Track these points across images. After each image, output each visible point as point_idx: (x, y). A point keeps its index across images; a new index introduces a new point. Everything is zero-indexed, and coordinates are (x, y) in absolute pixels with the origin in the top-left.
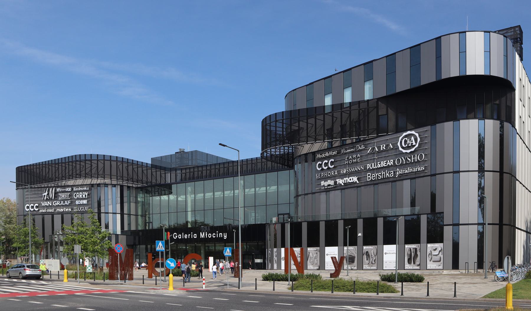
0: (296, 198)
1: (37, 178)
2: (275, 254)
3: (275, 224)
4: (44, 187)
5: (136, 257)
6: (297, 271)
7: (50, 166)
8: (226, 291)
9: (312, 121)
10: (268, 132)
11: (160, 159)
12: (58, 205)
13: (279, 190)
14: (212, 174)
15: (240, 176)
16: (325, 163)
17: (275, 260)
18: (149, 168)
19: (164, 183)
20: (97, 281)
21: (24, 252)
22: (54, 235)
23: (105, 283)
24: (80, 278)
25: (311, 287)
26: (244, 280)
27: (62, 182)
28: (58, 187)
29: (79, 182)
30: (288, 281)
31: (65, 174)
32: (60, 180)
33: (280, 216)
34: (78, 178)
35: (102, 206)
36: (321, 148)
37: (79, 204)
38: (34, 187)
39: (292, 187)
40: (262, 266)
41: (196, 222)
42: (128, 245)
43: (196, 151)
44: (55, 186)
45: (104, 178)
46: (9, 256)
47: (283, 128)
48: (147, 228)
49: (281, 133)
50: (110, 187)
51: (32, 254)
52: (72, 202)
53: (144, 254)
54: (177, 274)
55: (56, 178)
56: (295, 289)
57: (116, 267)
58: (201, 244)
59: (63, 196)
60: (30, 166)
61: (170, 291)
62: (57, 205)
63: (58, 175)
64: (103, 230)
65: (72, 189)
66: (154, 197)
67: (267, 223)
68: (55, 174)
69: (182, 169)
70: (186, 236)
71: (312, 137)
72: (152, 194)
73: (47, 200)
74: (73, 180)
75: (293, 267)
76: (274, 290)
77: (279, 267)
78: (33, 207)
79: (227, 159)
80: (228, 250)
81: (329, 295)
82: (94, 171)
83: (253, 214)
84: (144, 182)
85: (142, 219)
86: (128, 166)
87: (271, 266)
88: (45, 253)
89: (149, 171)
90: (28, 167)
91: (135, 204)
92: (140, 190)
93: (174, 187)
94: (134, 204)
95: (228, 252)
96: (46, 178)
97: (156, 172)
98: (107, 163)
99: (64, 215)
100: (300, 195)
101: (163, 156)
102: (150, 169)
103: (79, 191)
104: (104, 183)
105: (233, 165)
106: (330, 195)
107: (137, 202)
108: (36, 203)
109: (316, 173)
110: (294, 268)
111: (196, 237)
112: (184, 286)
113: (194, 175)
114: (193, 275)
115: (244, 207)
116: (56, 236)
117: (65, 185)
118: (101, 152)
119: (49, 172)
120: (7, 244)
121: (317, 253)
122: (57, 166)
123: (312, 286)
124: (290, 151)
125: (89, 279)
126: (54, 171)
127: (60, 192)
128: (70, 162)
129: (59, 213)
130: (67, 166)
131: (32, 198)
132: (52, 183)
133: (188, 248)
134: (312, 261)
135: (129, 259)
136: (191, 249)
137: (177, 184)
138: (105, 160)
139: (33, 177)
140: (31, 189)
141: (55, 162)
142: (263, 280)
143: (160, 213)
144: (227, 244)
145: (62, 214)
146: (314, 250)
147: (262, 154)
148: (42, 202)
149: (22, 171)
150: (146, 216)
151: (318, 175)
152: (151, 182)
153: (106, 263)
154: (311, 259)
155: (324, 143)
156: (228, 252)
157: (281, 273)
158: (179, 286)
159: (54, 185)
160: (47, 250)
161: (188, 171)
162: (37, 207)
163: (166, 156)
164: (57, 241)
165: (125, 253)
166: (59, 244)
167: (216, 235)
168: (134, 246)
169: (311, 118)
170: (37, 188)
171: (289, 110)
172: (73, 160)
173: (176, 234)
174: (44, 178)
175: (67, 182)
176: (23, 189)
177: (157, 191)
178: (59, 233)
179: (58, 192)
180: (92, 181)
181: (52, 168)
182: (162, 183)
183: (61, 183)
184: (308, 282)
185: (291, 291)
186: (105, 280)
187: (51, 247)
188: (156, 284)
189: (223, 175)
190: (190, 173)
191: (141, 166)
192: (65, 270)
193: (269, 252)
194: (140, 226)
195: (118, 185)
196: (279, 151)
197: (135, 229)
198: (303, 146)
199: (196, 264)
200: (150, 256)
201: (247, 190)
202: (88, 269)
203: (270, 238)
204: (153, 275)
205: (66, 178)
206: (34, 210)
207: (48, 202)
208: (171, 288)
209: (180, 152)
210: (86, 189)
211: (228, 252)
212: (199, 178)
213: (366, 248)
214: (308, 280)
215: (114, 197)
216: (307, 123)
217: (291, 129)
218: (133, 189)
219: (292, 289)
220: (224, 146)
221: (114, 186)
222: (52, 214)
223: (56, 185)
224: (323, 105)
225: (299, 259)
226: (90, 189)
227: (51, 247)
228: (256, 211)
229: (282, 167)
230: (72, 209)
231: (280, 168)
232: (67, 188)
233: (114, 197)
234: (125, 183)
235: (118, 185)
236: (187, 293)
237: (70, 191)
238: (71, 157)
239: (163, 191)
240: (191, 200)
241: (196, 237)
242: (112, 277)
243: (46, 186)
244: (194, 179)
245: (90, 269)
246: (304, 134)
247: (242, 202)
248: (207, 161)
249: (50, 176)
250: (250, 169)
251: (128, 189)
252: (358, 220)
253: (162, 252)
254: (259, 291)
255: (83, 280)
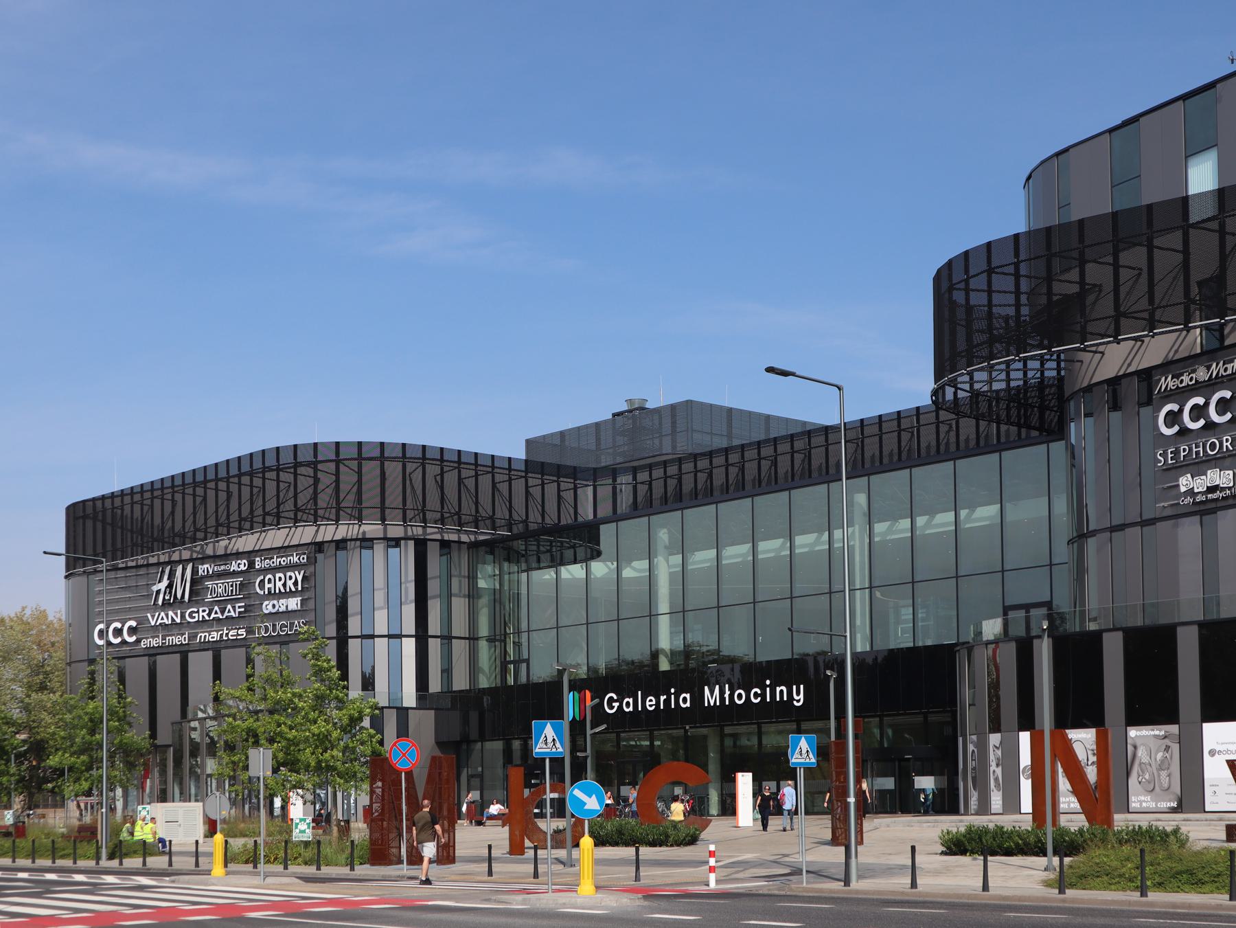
0: (1075, 545)
1: (135, 536)
2: (993, 756)
3: (996, 642)
4: (158, 564)
5: (468, 784)
6: (1083, 817)
7: (176, 492)
8: (798, 894)
9: (1134, 257)
10: (961, 314)
11: (558, 442)
12: (204, 621)
13: (1010, 517)
14: (748, 478)
15: (847, 479)
16: (1195, 407)
17: (996, 779)
18: (516, 473)
19: (570, 521)
20: (326, 870)
21: (86, 780)
22: (189, 721)
23: (356, 875)
24: (268, 862)
25: (1139, 878)
26: (866, 855)
27: (218, 542)
28: (204, 559)
29: (275, 537)
30: (1045, 855)
31: (228, 516)
32: (209, 535)
33: (1012, 614)
34: (271, 525)
35: (353, 615)
36: (1176, 351)
37: (274, 611)
38: (124, 565)
39: (1061, 506)
40: (946, 803)
41: (687, 653)
42: (440, 744)
43: (687, 401)
44: (195, 556)
45: (360, 520)
46: (38, 797)
47: (1018, 293)
48: (511, 681)
49: (1011, 311)
50: (379, 548)
51: (112, 789)
52: (249, 606)
53: (500, 771)
54: (615, 837)
55: (197, 530)
56: (1072, 886)
57: (396, 820)
58: (707, 729)
59: (220, 590)
60: (110, 500)
61: (585, 897)
62: (198, 621)
63: (202, 521)
64: (355, 692)
65: (251, 564)
66: (535, 575)
67: (960, 641)
68: (195, 517)
69: (635, 471)
70: (651, 701)
71: (1136, 315)
72: (526, 561)
73: (166, 605)
74: (252, 534)
75: (1068, 801)
76: (985, 887)
77: (1012, 804)
78: (118, 632)
79: (805, 423)
80: (803, 744)
81: (1219, 907)
82: (324, 499)
83: (907, 613)
84: (498, 523)
85: (493, 649)
86: (442, 474)
87: (979, 800)
88: (157, 781)
89: (518, 486)
90: (125, 498)
91: (467, 600)
92: (486, 552)
93: (607, 533)
94: (463, 599)
95: (802, 752)
96: (163, 533)
97: (543, 484)
98: (371, 471)
99: (223, 652)
100: (1093, 533)
101: (570, 430)
102: (522, 477)
103: (273, 570)
104: (360, 536)
105: (827, 440)
106: (1219, 523)
107: (473, 594)
108: (130, 619)
109: (1156, 448)
110: (1072, 805)
111: (688, 704)
112: (637, 878)
113: (681, 486)
114: (676, 841)
115: (871, 588)
116: (193, 724)
117: (229, 552)
118: (349, 434)
119: (173, 513)
120: (34, 759)
121: (1167, 748)
122: (286, 477)
123: (1143, 873)
124: (1047, 374)
125: (299, 864)
126: (189, 510)
127: (211, 576)
128: (245, 474)
129: (205, 646)
130: (234, 488)
131: (118, 601)
132: (185, 549)
133: (657, 743)
134: (1147, 776)
135: (440, 788)
136: (670, 747)
137: (617, 521)
138: (365, 459)
139: (122, 533)
140: (112, 575)
141: (194, 479)
142: (943, 853)
143: (557, 628)
144: (804, 726)
145: (216, 650)
146: (1155, 736)
147: (935, 393)
148: (149, 615)
149: (85, 517)
150: (508, 639)
151: (1164, 455)
152: (526, 522)
153: (364, 807)
154: (1143, 772)
155: (1188, 331)
156: (804, 751)
157: (1017, 825)
158: (619, 878)
159: (191, 555)
160: (163, 772)
161: (657, 473)
162: (132, 631)
163: (579, 428)
164: (199, 741)
165: (426, 771)
166: (204, 749)
167: (763, 695)
168: (464, 747)
169: (1130, 247)
170: (134, 570)
171: (1041, 225)
172: (254, 468)
173: (615, 697)
174: (158, 534)
175: (234, 540)
176: (90, 573)
177: (548, 551)
178: (204, 712)
179: (203, 577)
180: (317, 531)
181: (183, 498)
182: (563, 522)
183: (214, 546)
184: (1127, 859)
185: (1057, 891)
186: (356, 867)
187: (178, 762)
188: (536, 875)
189: (790, 480)
190: (696, 475)
191: (490, 469)
192: (216, 836)
193: (971, 747)
194: (483, 672)
195: (406, 539)
196: (1003, 376)
197: (468, 688)
198: (1103, 353)
199: (688, 802)
200: (517, 774)
201: (880, 528)
202: (298, 831)
203: (973, 697)
204: (527, 843)
205: (252, 522)
206: (124, 642)
207: (171, 613)
208: (587, 887)
209: (630, 411)
210: (296, 559)
211: (802, 752)
212: (700, 497)
213: (1139, 733)
214: (1126, 849)
215: (394, 581)
216: (1116, 266)
217: (1050, 293)
218: (459, 549)
219: (1062, 884)
220: (785, 373)
221: (396, 543)
222: (183, 653)
223: (198, 553)
224: (1181, 195)
225: (1092, 774)
226: (312, 561)
227: (178, 762)
228: (919, 600)
229: (1019, 434)
230: (250, 631)
231: (1012, 439)
232: (234, 562)
233: (394, 581)
234: (433, 533)
235: (406, 539)
236: (646, 903)
237: (242, 572)
238: (293, 448)
239: (569, 548)
240: (671, 574)
241: (688, 704)
242: (379, 854)
243: (163, 559)
244: (681, 501)
245: (303, 830)
246: (1106, 307)
247: (862, 569)
248: (730, 436)
249: (178, 527)
250: (874, 455)
251: (446, 551)
252: (1106, 637)
253: (557, 762)
254: (927, 894)
255: (280, 868)
